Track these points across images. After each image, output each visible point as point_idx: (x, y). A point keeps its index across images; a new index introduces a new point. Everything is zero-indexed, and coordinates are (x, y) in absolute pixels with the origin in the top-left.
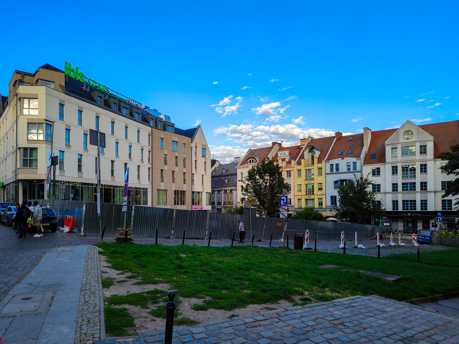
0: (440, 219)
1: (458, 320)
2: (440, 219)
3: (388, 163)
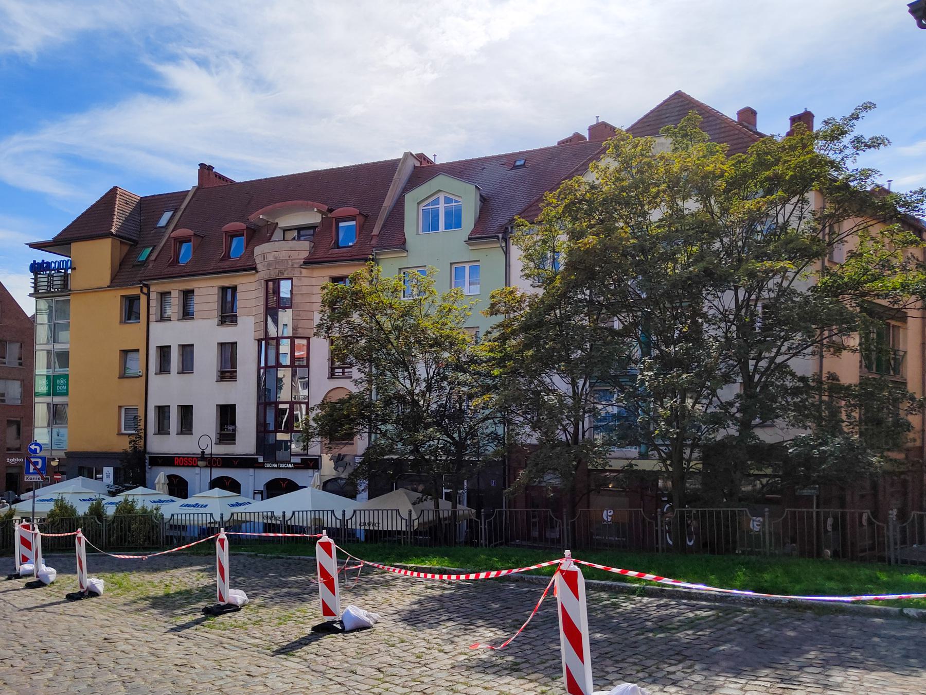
0: (36, 464)
2: (36, 464)
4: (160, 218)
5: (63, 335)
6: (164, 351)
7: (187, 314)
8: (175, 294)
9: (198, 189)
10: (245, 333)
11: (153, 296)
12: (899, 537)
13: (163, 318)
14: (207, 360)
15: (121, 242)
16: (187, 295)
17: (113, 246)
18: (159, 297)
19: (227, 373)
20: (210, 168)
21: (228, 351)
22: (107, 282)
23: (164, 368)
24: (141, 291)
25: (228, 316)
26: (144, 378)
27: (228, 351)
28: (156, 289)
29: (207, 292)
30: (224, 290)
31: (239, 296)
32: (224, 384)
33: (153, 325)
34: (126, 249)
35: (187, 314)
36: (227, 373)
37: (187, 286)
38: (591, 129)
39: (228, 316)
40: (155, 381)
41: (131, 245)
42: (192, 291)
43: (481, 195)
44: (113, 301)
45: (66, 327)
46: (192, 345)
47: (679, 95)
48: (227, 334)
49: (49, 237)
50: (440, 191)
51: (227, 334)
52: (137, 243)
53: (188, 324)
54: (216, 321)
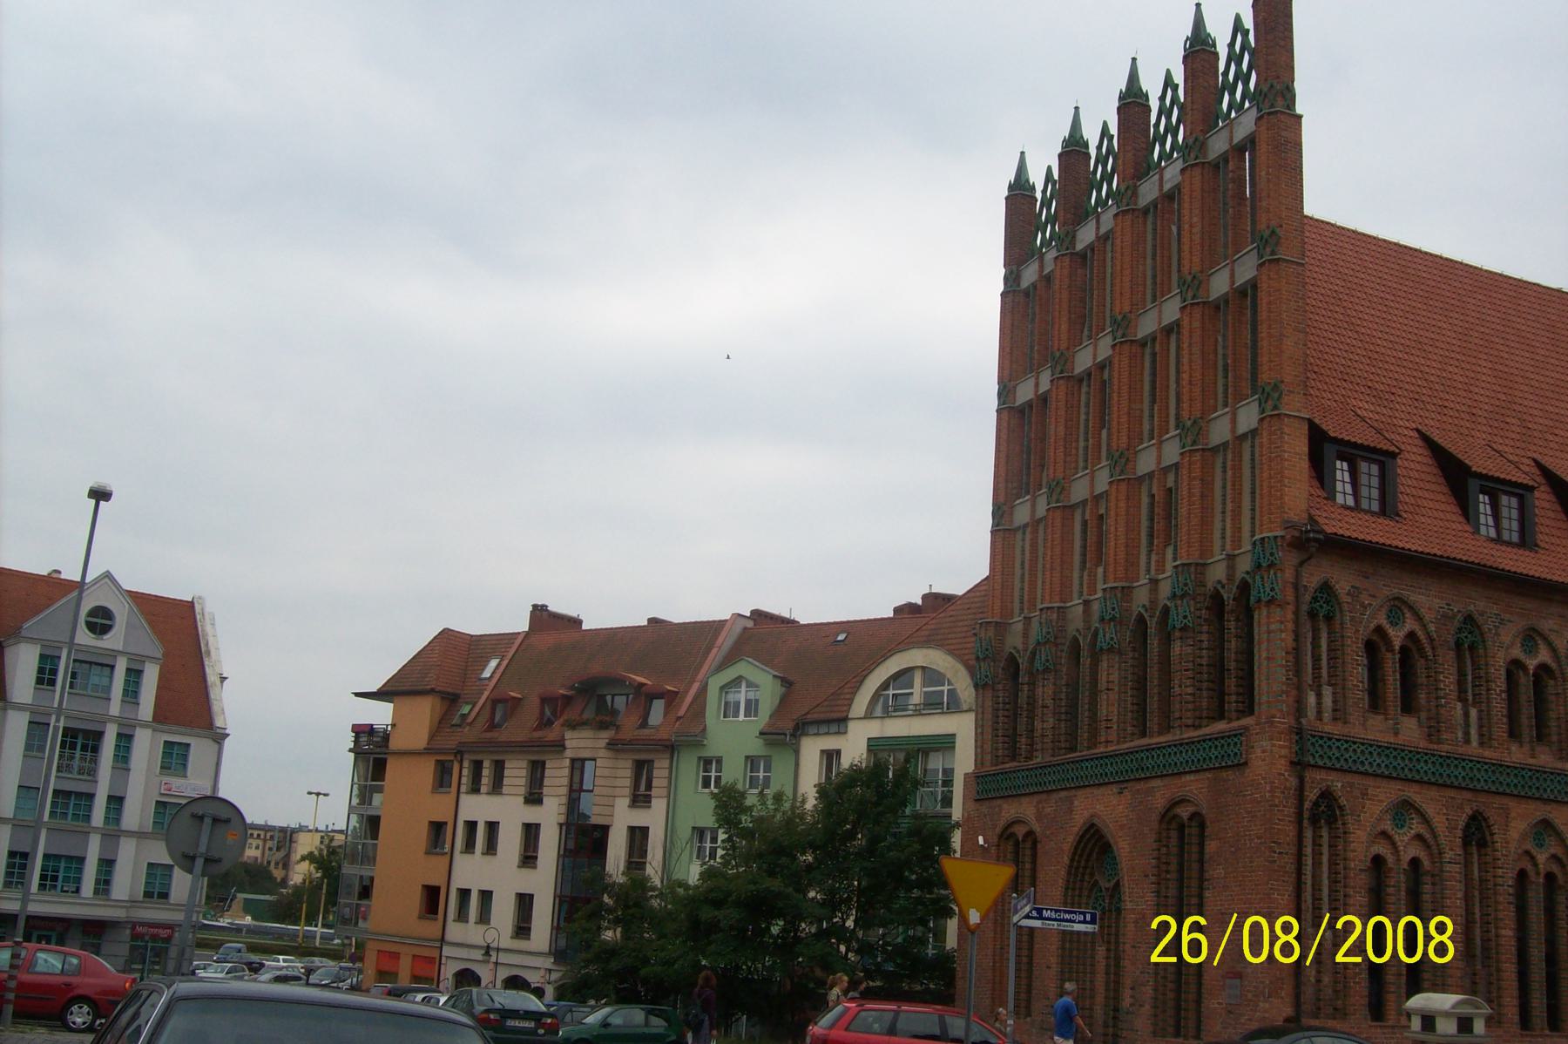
3: (20, 707)
4: (485, 666)
5: (377, 799)
6: (471, 826)
7: (497, 787)
8: (486, 764)
9: (527, 634)
10: (550, 815)
11: (466, 764)
12: (1122, 555)
13: (475, 789)
14: (511, 841)
19: (529, 859)
20: (543, 608)
21: (531, 832)
23: (469, 846)
25: (534, 798)
27: (531, 832)
32: (525, 871)
33: (463, 797)
35: (497, 787)
36: (529, 859)
38: (925, 597)
39: (534, 798)
40: (459, 859)
44: (426, 771)
45: (380, 790)
47: (446, 636)
48: (532, 814)
49: (374, 687)
51: (532, 814)
53: (495, 799)
54: (521, 799)
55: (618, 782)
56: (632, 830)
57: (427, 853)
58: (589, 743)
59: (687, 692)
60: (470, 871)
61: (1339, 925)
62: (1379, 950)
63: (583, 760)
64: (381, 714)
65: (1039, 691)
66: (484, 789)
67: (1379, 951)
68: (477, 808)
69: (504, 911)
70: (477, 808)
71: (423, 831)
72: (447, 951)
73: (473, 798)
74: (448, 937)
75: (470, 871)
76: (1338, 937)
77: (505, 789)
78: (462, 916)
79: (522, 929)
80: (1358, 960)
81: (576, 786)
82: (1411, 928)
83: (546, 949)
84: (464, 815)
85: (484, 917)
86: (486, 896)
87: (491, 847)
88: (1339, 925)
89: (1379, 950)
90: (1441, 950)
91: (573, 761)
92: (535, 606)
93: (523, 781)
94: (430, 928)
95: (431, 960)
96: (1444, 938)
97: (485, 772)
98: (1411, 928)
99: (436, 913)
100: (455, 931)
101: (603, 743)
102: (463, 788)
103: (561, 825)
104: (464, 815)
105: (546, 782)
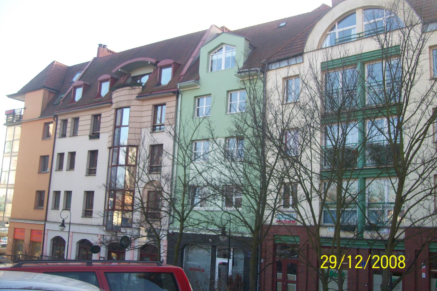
1: (345, 286)
6: (61, 155)
8: (70, 121)
10: (102, 145)
11: (59, 122)
13: (64, 135)
14: (82, 161)
15: (50, 92)
16: (76, 120)
17: (44, 92)
18: (62, 123)
19: (91, 170)
20: (75, 155)
21: (93, 154)
22: (39, 115)
23: (60, 168)
24: (54, 119)
25: (95, 135)
26: (49, 173)
28: (60, 118)
29: (85, 121)
30: (156, 107)
31: (80, 123)
33: (57, 140)
34: (52, 96)
35: (74, 134)
36: (91, 170)
37: (75, 116)
40: (56, 175)
41: (56, 94)
42: (100, 115)
43: (250, 44)
46: (71, 192)
48: (93, 145)
49: (16, 92)
50: (222, 44)
51: (93, 145)
52: (59, 92)
55: (144, 114)
56: (153, 147)
57: (39, 173)
58: (127, 98)
59: (185, 64)
60: (61, 181)
61: (373, 258)
62: (384, 265)
63: (122, 108)
64: (18, 106)
65: (359, 112)
66: (68, 134)
67: (384, 265)
68: (64, 145)
69: (78, 202)
70: (64, 145)
71: (37, 161)
72: (48, 226)
73: (63, 139)
74: (48, 219)
75: (61, 181)
76: (362, 264)
77: (79, 133)
78: (56, 206)
79: (88, 212)
80: (379, 267)
81: (118, 124)
82: (393, 259)
83: (101, 223)
84: (58, 150)
85: (67, 207)
86: (69, 194)
87: (72, 166)
88: (373, 258)
89: (384, 265)
90: (402, 265)
91: (117, 110)
92: (100, 45)
93: (89, 127)
94: (40, 214)
95: (39, 232)
96: (403, 261)
97: (69, 125)
98: (393, 259)
99: (43, 206)
100: (53, 215)
101: (134, 97)
102: (58, 136)
103: (110, 148)
104: (58, 150)
105: (102, 125)
